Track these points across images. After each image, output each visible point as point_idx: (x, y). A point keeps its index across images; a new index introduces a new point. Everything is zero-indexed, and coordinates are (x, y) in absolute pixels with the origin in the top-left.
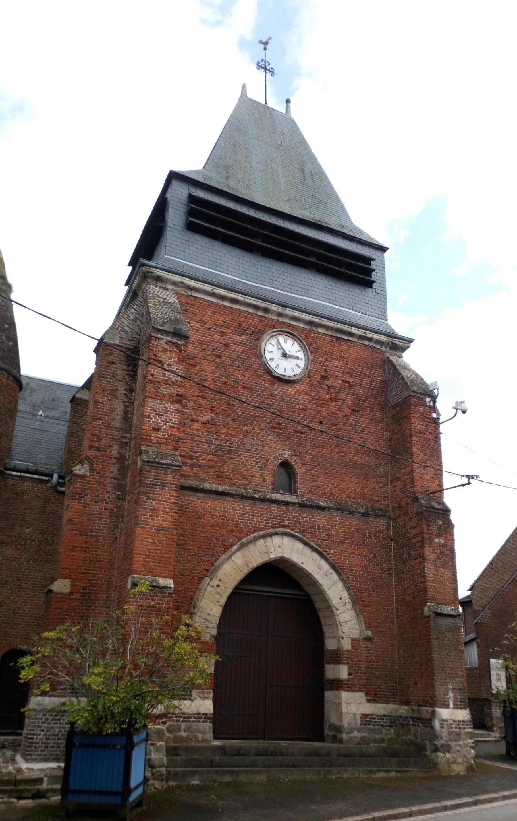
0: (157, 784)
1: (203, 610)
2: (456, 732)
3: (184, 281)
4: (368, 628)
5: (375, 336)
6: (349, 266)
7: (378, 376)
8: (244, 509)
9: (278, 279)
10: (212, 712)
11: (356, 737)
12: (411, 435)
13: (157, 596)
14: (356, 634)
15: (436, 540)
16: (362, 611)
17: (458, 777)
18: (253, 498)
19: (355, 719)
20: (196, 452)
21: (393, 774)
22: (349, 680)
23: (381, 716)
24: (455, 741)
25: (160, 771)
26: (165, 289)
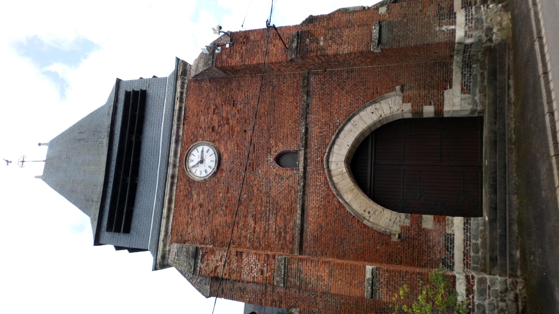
0: (520, 287)
1: (387, 225)
2: (475, 23)
3: (162, 239)
4: (393, 89)
5: (179, 90)
6: (134, 109)
7: (207, 85)
8: (313, 193)
9: (151, 165)
10: (462, 218)
11: (480, 98)
12: (244, 65)
13: (379, 280)
14: (399, 99)
15: (321, 43)
16: (381, 94)
17: (514, 20)
18: (304, 187)
19: (465, 99)
20: (276, 229)
21: (511, 82)
22: (435, 105)
23: (462, 76)
24: (482, 23)
25: (510, 285)
26: (169, 251)
